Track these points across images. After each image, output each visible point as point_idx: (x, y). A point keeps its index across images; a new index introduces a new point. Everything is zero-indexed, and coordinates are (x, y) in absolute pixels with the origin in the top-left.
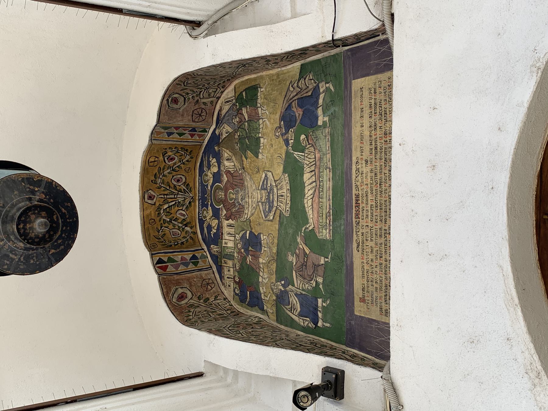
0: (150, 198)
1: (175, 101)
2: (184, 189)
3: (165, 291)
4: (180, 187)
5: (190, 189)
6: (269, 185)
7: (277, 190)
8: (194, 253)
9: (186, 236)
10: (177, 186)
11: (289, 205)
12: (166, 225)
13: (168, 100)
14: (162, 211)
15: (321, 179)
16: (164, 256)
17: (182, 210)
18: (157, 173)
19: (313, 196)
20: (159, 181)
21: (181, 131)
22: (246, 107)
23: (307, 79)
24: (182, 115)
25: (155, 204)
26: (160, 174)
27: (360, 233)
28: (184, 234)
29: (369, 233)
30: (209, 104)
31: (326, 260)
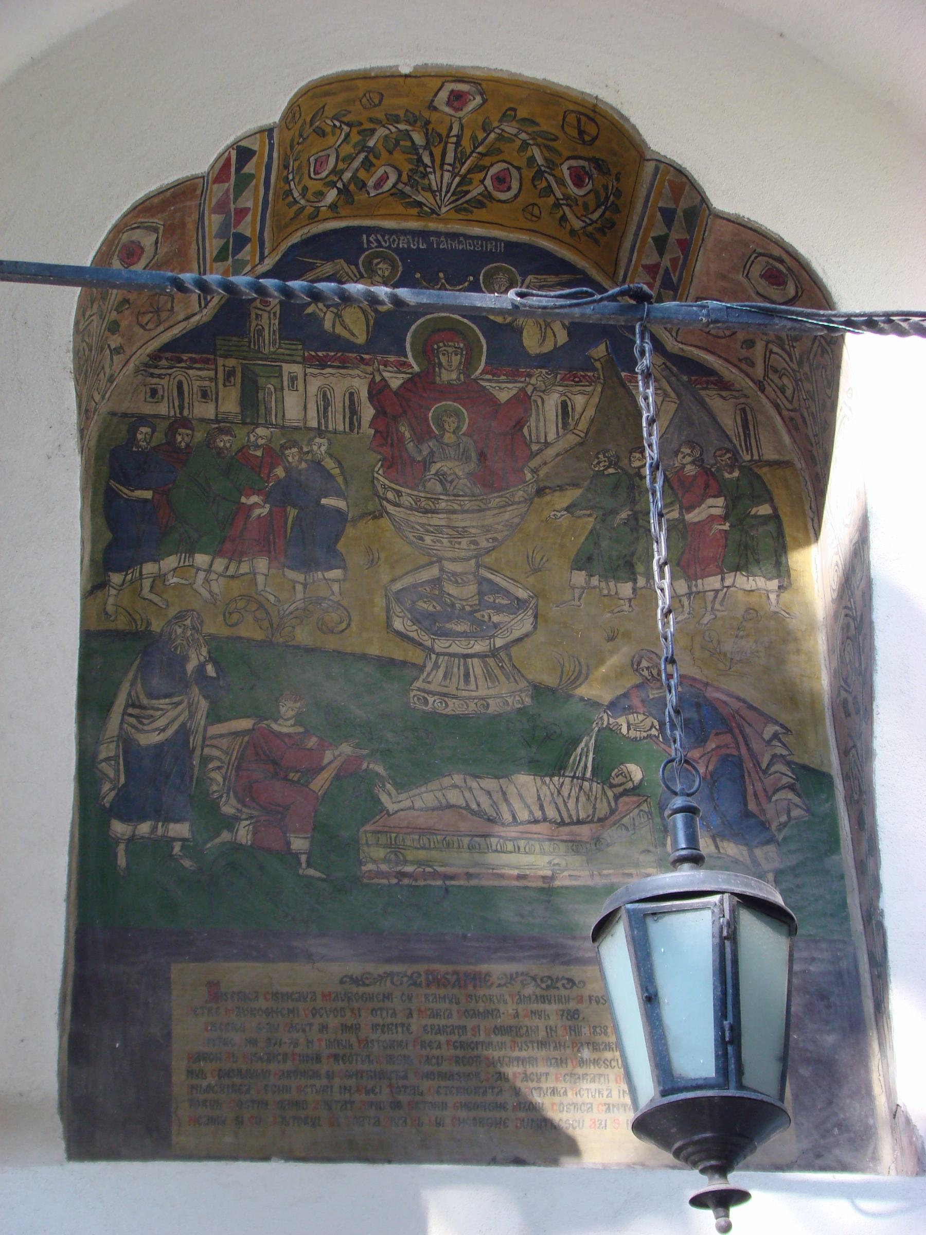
0: (457, 99)
1: (774, 277)
2: (467, 192)
3: (156, 200)
4: (476, 182)
5: (465, 210)
6: (495, 619)
7: (482, 656)
8: (256, 240)
9: (309, 195)
10: (482, 175)
11: (440, 708)
12: (355, 138)
13: (781, 261)
14: (402, 127)
15: (522, 843)
16: (258, 165)
17: (399, 180)
18: (536, 129)
19: (473, 813)
20: (510, 129)
21: (673, 251)
22: (725, 518)
23: (791, 795)
24: (723, 277)
25: (432, 108)
26: (533, 136)
27: (387, 987)
28: (314, 186)
29: (393, 1020)
30: (744, 352)
31: (303, 858)
